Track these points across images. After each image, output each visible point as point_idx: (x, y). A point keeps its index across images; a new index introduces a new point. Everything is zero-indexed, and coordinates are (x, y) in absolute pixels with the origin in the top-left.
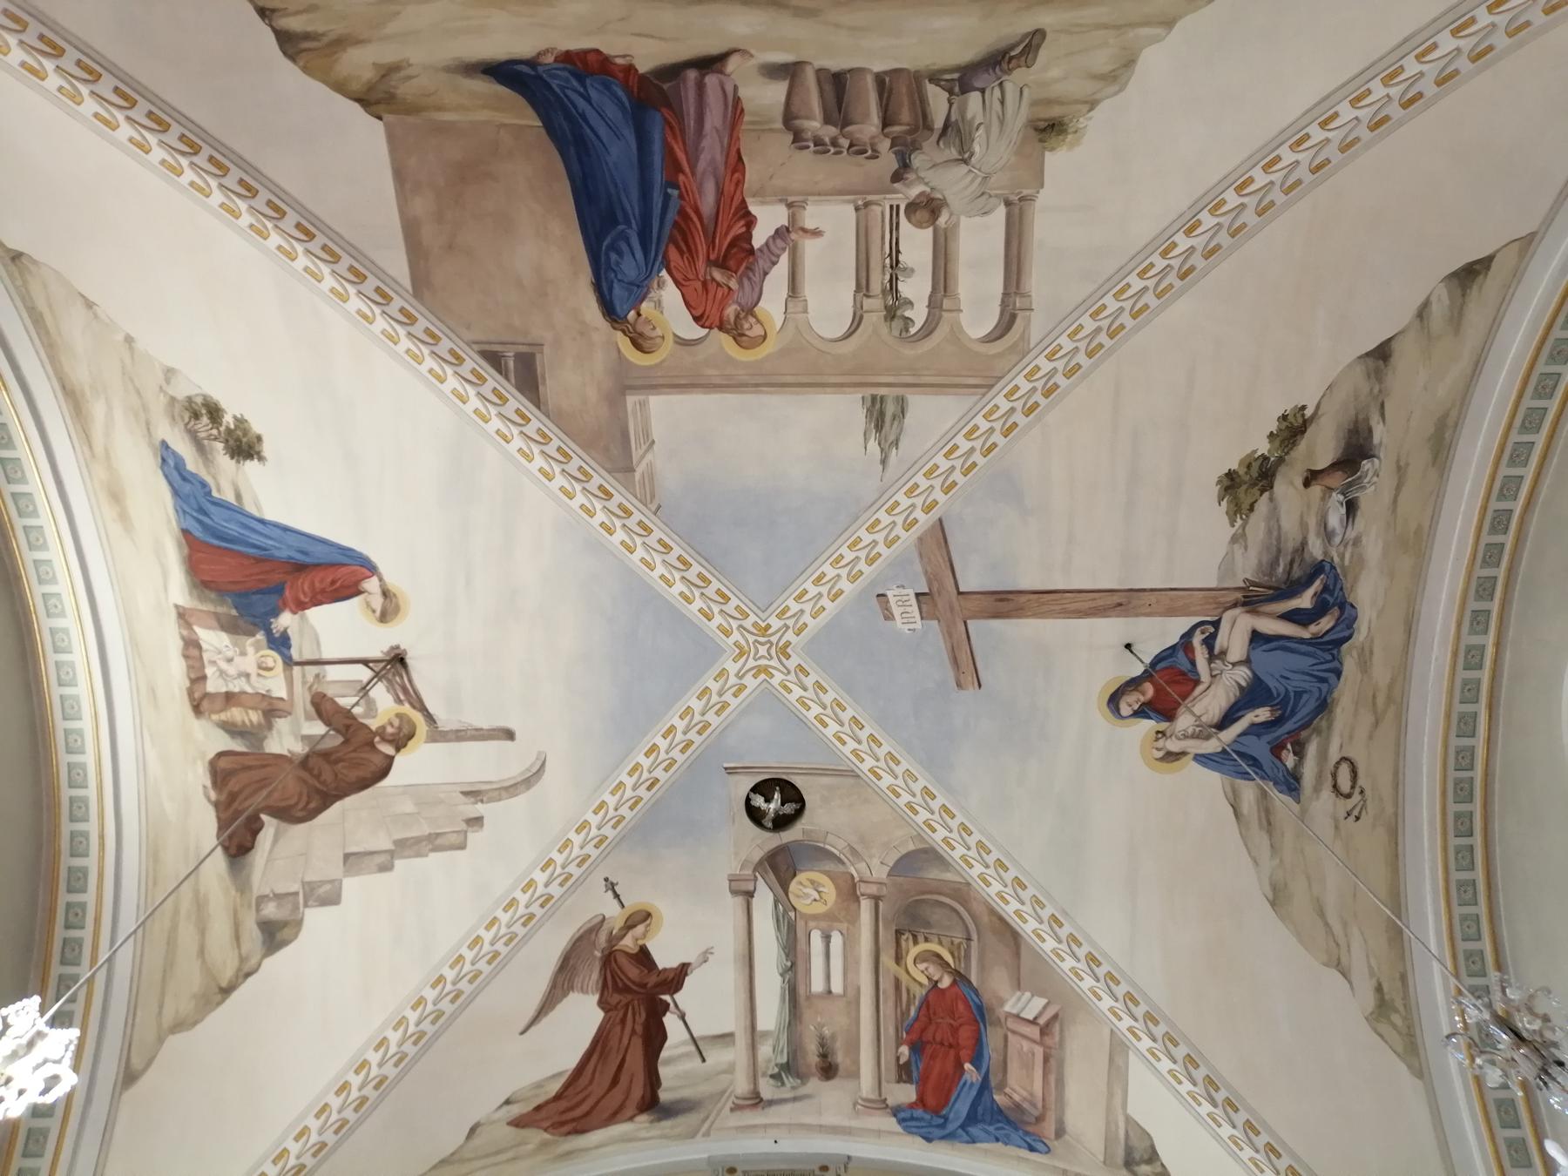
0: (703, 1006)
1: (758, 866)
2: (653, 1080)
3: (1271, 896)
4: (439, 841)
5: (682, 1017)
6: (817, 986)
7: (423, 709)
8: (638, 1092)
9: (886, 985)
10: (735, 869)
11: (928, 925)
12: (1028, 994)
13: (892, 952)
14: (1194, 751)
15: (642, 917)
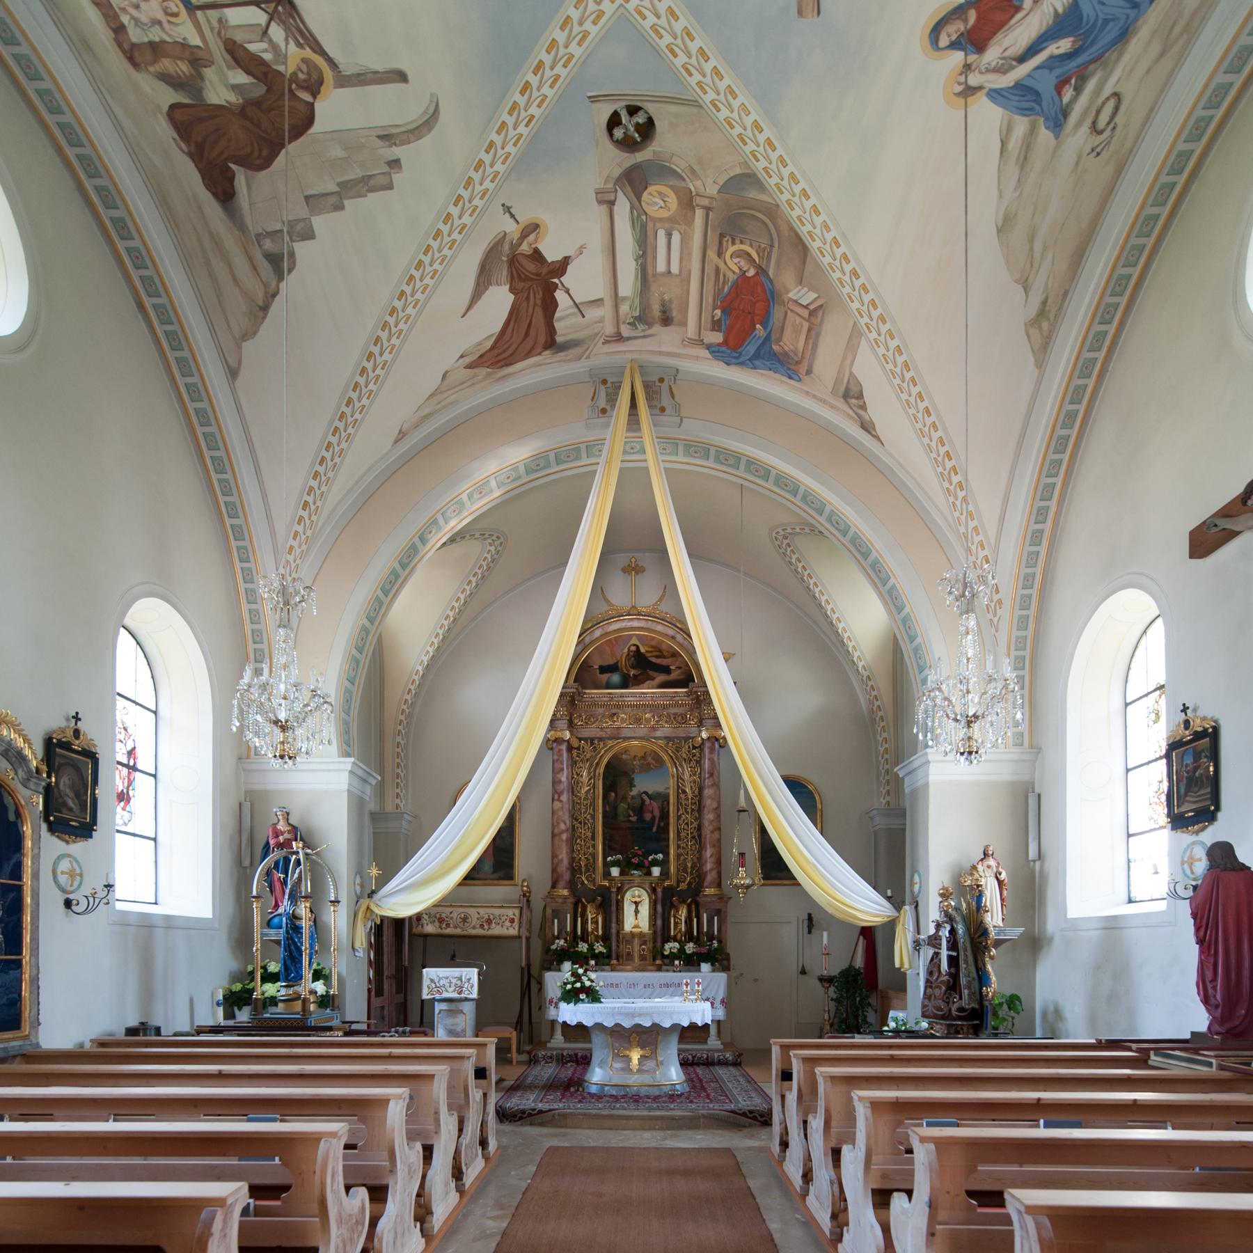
0: (583, 283)
1: (618, 181)
2: (551, 331)
3: (1000, 225)
4: (372, 182)
5: (567, 291)
6: (661, 267)
7: (323, 53)
8: (542, 339)
9: (710, 270)
10: (600, 184)
11: (743, 231)
12: (806, 289)
13: (716, 248)
14: (988, 86)
15: (533, 228)
